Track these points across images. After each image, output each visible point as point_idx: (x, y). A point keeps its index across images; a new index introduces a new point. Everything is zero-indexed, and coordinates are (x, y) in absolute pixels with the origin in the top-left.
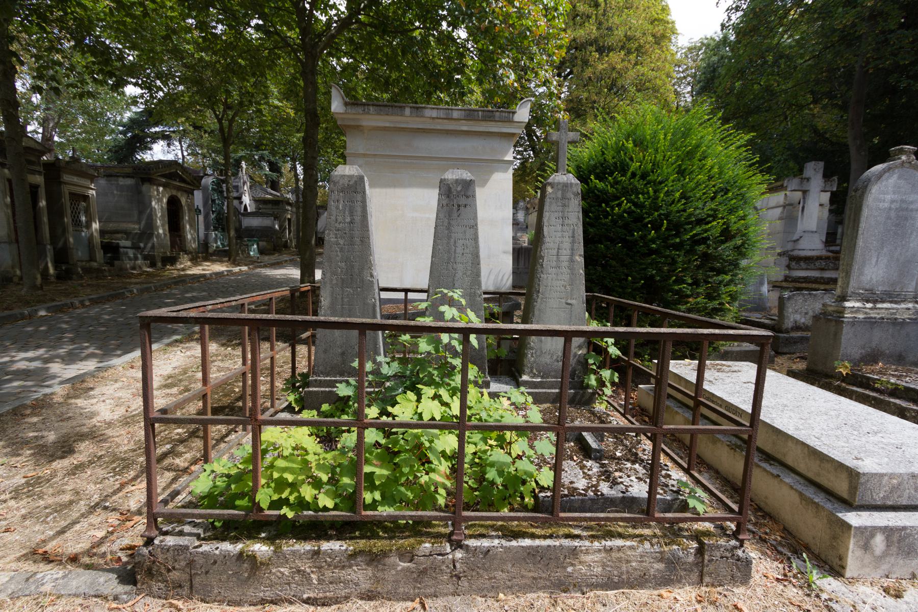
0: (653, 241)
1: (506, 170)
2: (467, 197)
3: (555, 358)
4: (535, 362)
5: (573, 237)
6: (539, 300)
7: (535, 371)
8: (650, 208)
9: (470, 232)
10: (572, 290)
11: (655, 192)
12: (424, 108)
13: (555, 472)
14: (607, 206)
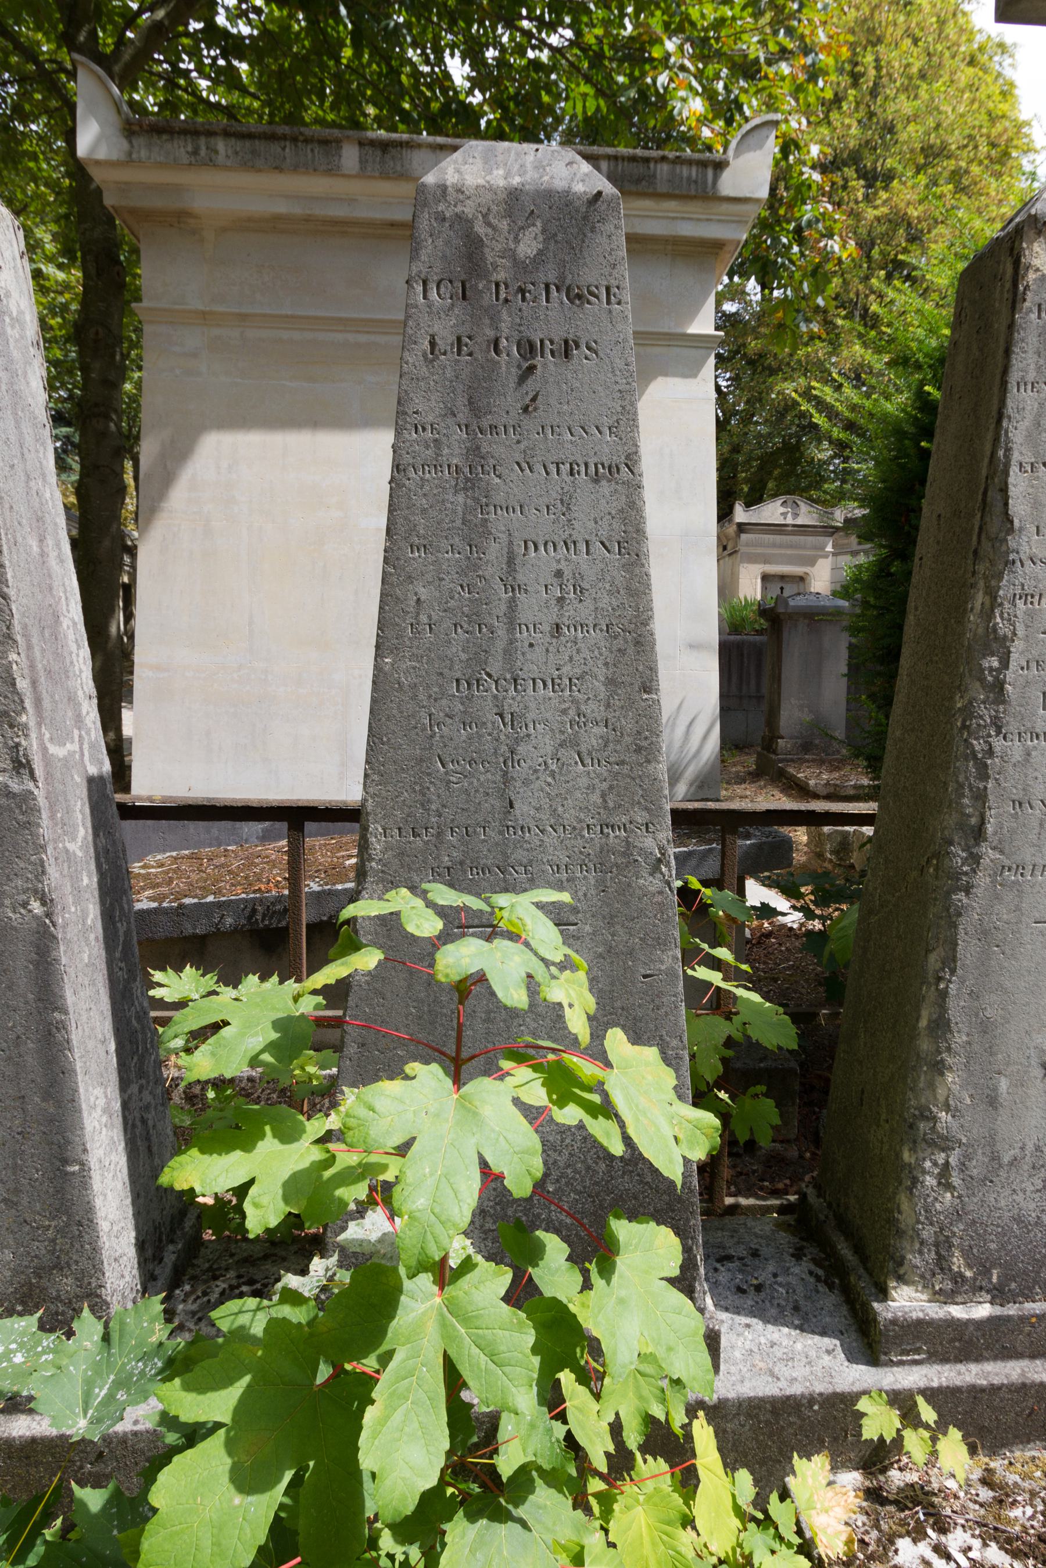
1: (691, 371)
2: (577, 297)
4: (958, 1214)
6: (982, 880)
7: (958, 1262)
9: (593, 504)
12: (407, 145)
13: (236, 88)
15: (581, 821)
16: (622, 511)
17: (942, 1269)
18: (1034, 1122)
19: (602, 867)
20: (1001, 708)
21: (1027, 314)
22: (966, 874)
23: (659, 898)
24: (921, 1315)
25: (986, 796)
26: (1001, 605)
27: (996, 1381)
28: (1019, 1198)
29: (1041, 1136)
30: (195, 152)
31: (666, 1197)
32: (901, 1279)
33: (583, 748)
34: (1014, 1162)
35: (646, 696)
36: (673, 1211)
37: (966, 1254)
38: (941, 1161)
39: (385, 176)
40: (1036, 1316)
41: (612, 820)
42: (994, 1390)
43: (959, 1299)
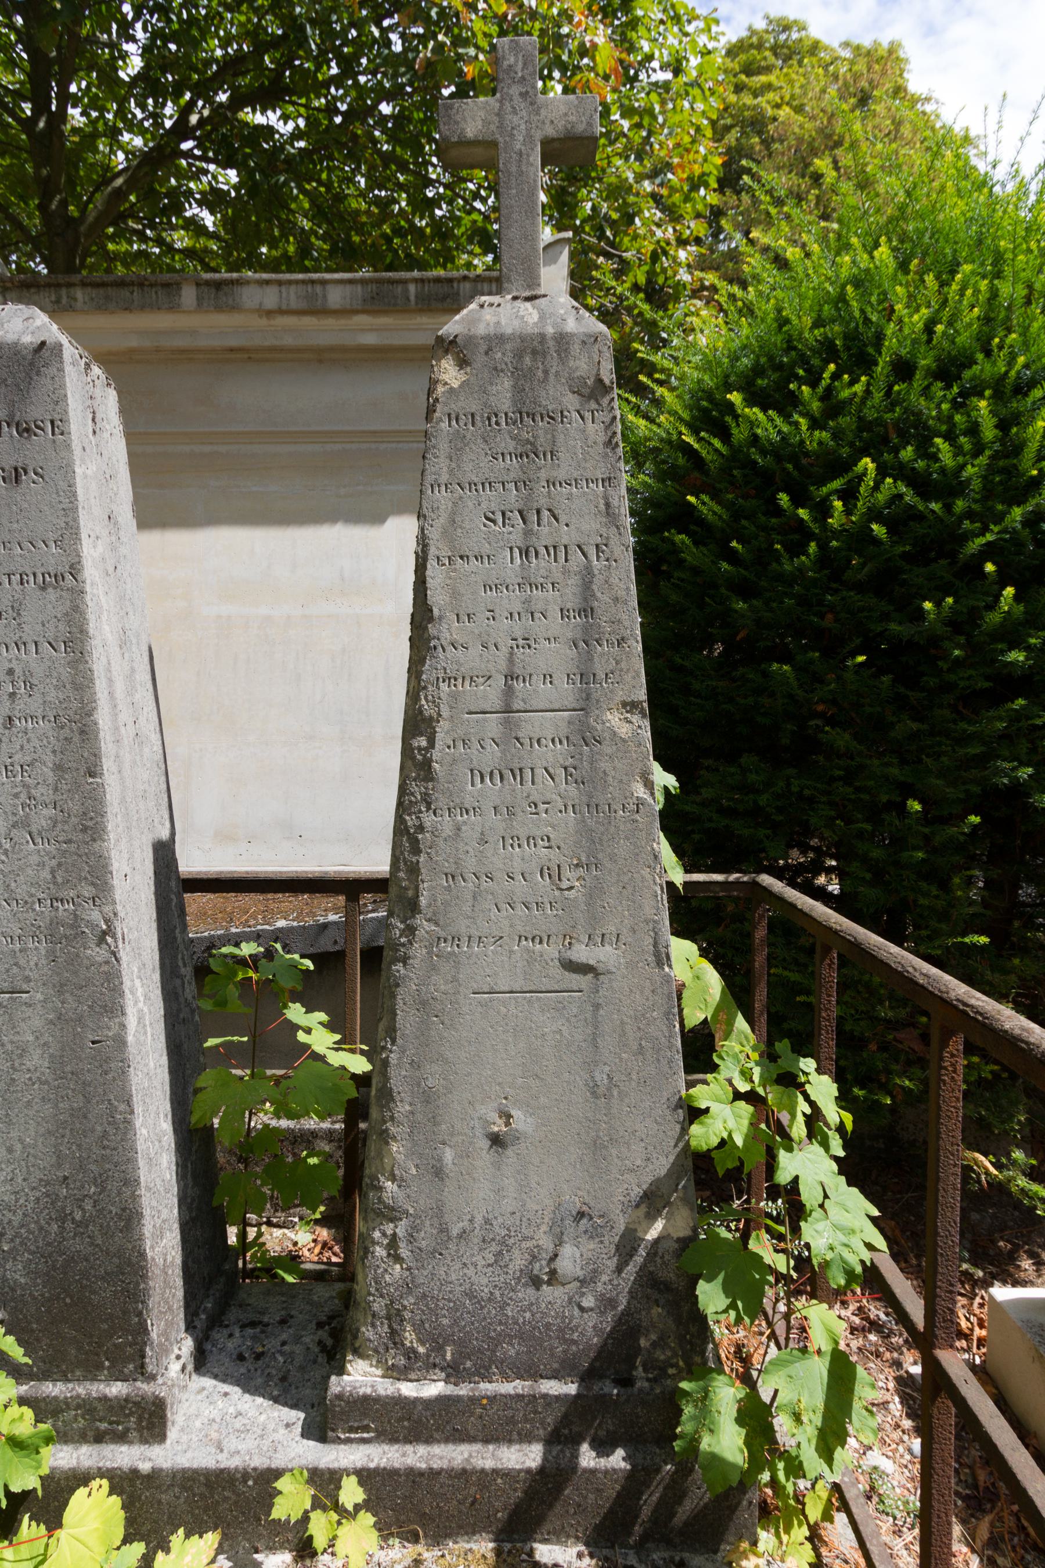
0: (1011, 634)
2: (25, 431)
3: (518, 1261)
4: (408, 1287)
5: (586, 611)
6: (418, 951)
7: (409, 1337)
8: (988, 492)
9: (41, 610)
10: (594, 893)
11: (1003, 425)
12: (232, 282)
14: (798, 501)
15: (32, 895)
16: (67, 614)
17: (395, 1343)
18: (481, 1195)
19: (52, 938)
20: (430, 785)
21: (437, 423)
22: (403, 945)
23: (105, 968)
24: (369, 1391)
25: (419, 870)
26: (425, 688)
27: (436, 1465)
28: (470, 1272)
29: (490, 1209)
30: (58, 301)
31: (116, 1260)
32: (358, 1353)
33: (34, 829)
34: (463, 1235)
35: (91, 780)
36: (123, 1274)
37: (418, 1328)
38: (389, 1232)
39: (219, 309)
40: (488, 1397)
41: (61, 895)
42: (433, 1474)
43: (413, 1376)
